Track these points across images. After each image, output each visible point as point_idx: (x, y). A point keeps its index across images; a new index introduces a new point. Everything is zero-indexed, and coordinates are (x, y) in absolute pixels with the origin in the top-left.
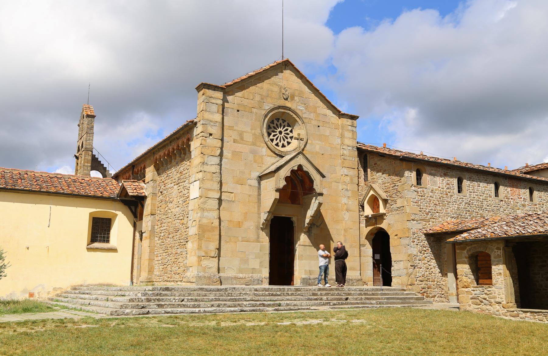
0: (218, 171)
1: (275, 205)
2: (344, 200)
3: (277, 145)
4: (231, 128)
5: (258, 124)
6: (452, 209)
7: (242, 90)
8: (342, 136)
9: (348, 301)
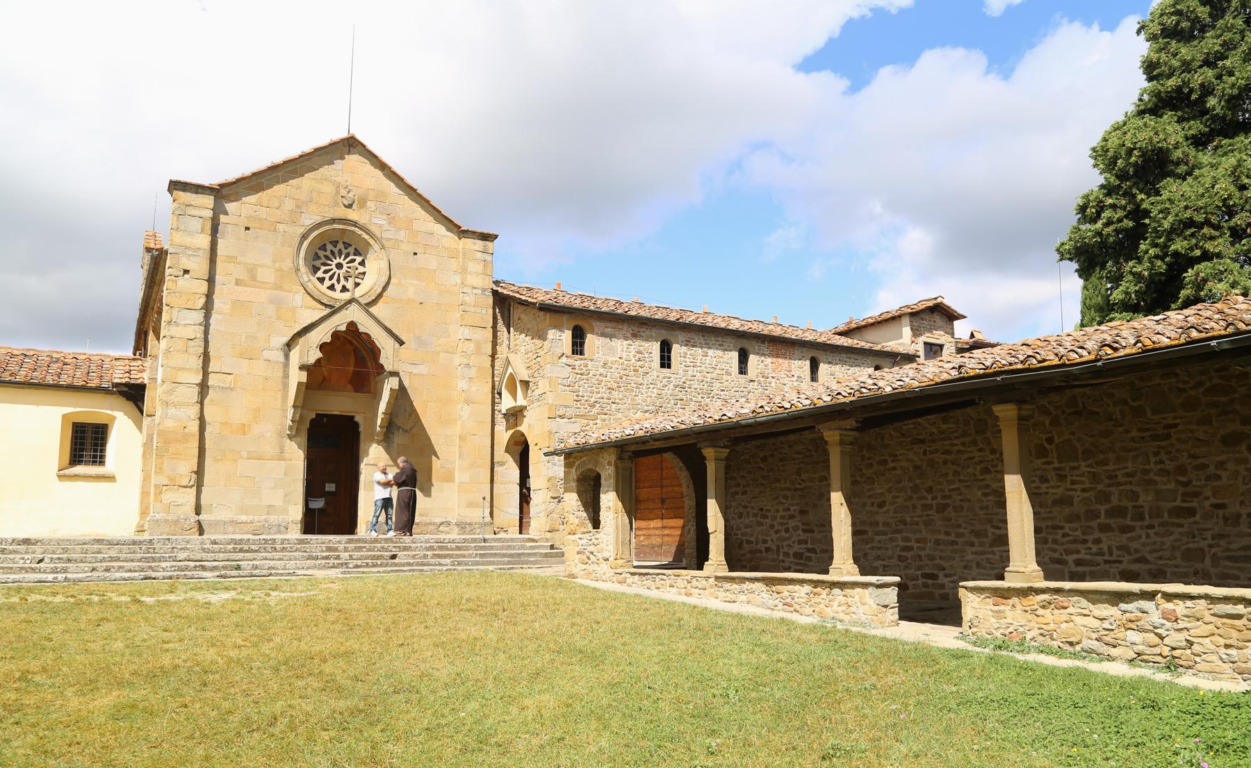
0: (200, 335)
1: (302, 395)
2: (462, 384)
3: (332, 288)
4: (231, 259)
5: (289, 251)
6: (646, 396)
7: (257, 192)
8: (464, 270)
9: (396, 561)
